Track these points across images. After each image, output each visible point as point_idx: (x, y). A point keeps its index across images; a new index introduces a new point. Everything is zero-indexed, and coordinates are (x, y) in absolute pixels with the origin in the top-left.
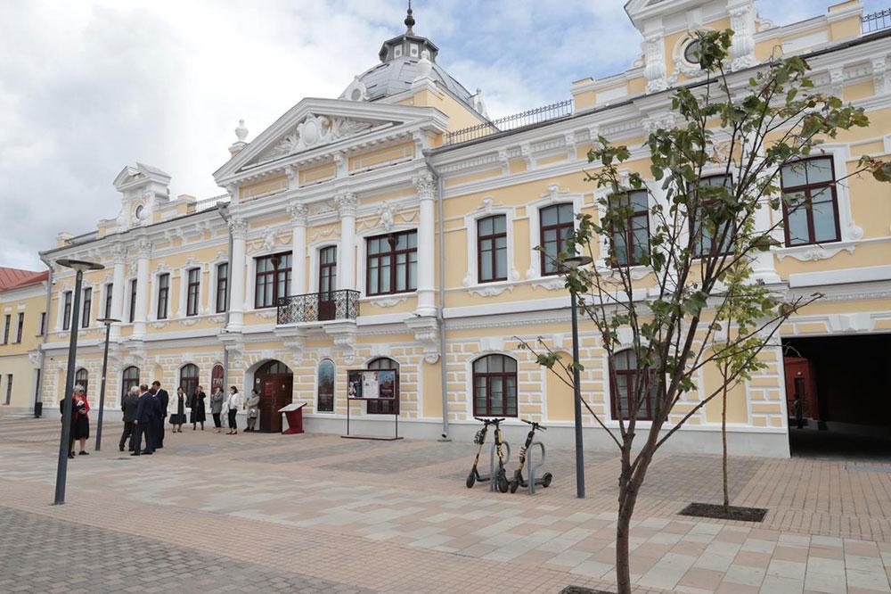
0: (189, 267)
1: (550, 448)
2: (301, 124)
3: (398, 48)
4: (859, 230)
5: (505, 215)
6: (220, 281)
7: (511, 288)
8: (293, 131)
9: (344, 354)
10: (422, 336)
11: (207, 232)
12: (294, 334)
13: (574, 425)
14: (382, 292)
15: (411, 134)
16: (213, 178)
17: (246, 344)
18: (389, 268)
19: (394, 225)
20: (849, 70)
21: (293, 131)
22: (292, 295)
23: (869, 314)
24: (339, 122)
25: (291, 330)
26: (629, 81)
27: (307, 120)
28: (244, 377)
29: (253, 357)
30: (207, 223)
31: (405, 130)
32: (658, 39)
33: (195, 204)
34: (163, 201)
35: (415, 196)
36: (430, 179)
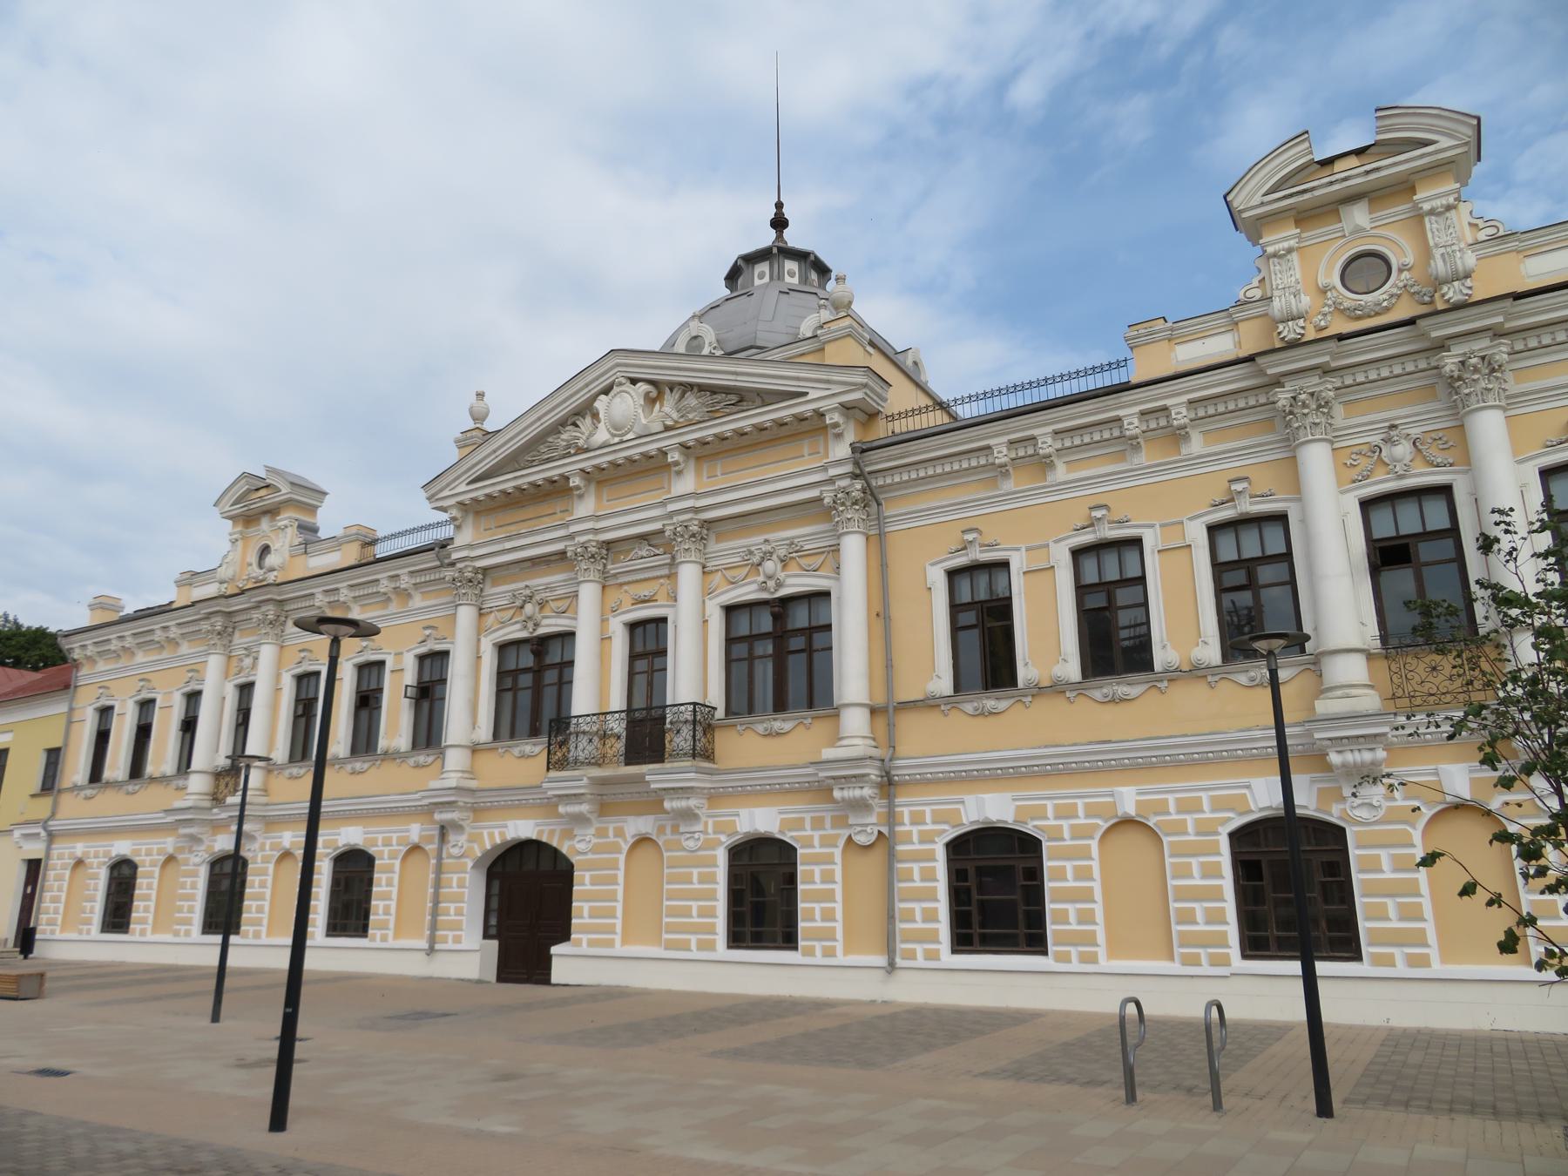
0: (299, 670)
2: (602, 397)
3: (763, 267)
8: (586, 410)
9: (851, 821)
11: (404, 595)
13: (1300, 973)
15: (567, 479)
16: (423, 495)
18: (529, 692)
20: (1147, 417)
21: (586, 410)
23: (1009, 795)
24: (676, 394)
28: (467, 876)
29: (491, 836)
30: (90, 648)
32: (1290, 251)
33: (374, 542)
34: (310, 537)
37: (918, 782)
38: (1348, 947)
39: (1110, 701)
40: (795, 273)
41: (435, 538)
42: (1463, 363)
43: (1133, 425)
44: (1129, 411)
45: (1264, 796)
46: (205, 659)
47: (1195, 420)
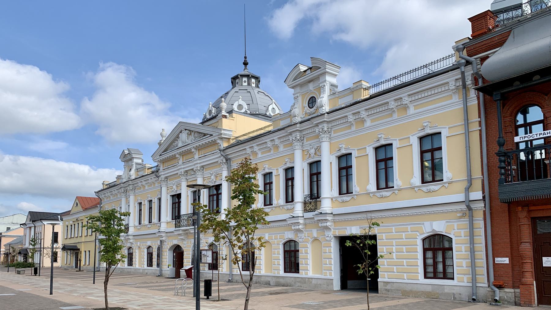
5: (440, 133)
6: (287, 180)
7: (446, 185)
10: (323, 225)
12: (181, 233)
14: (436, 179)
16: (152, 158)
17: (334, 221)
18: (291, 186)
19: (216, 181)
20: (397, 101)
21: (178, 137)
22: (181, 214)
25: (179, 231)
26: (353, 92)
27: (183, 132)
31: (214, 138)
35: (318, 140)
36: (224, 161)
39: (381, 197)
40: (246, 81)
41: (394, 84)
46: (221, 173)
47: (428, 96)
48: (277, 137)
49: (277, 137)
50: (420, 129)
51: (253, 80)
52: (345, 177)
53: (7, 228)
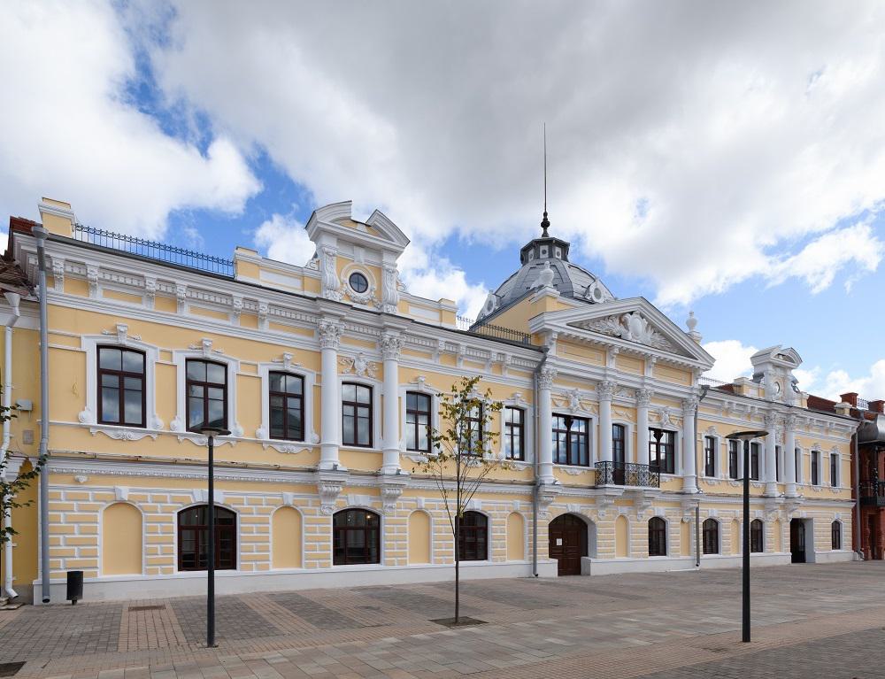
1: (221, 602)
4: (241, 430)
20: (272, 307)
37: (59, 473)
38: (232, 565)
42: (328, 326)
43: (442, 346)
44: (239, 297)
45: (199, 496)
48: (466, 344)
49: (466, 344)
50: (107, 332)
51: (558, 250)
52: (124, 353)
53: (270, 372)
